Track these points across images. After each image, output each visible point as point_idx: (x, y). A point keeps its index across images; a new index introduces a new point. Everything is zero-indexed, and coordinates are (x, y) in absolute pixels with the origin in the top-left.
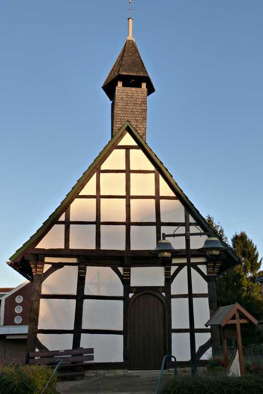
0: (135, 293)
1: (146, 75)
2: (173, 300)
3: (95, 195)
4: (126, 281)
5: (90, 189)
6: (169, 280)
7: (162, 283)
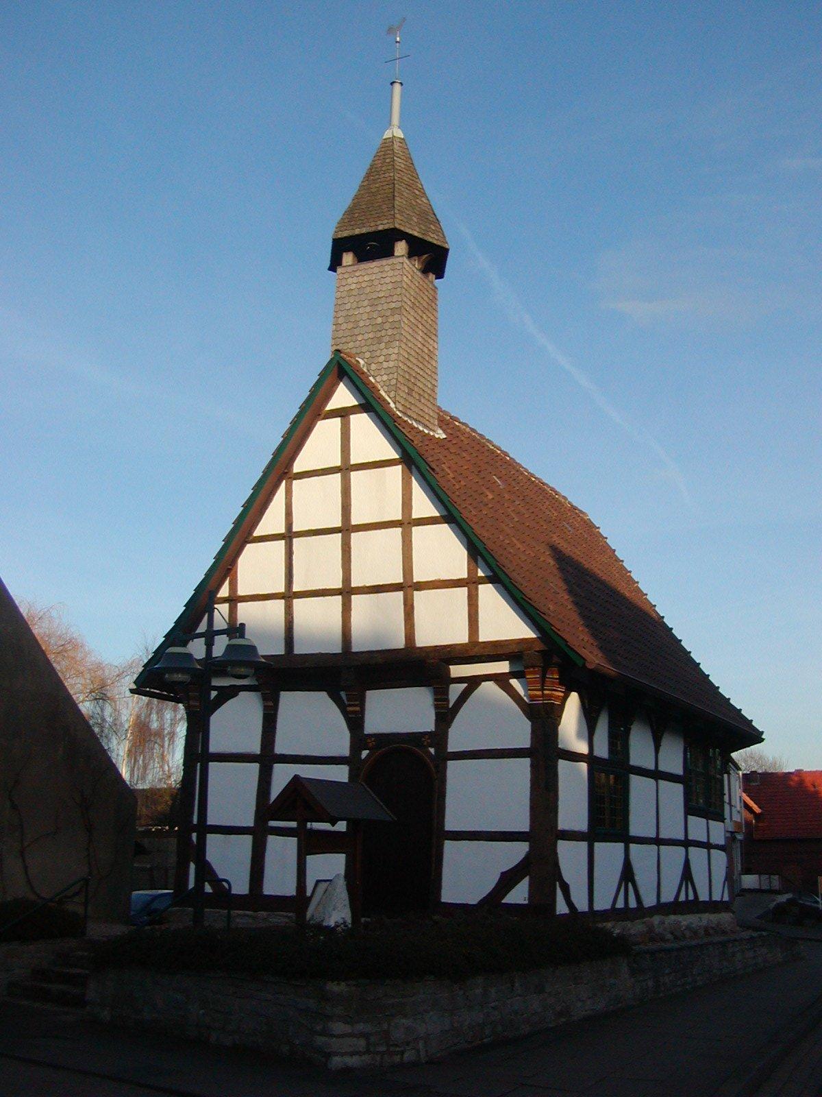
2: (451, 764)
3: (400, 518)
4: (355, 722)
5: (272, 521)
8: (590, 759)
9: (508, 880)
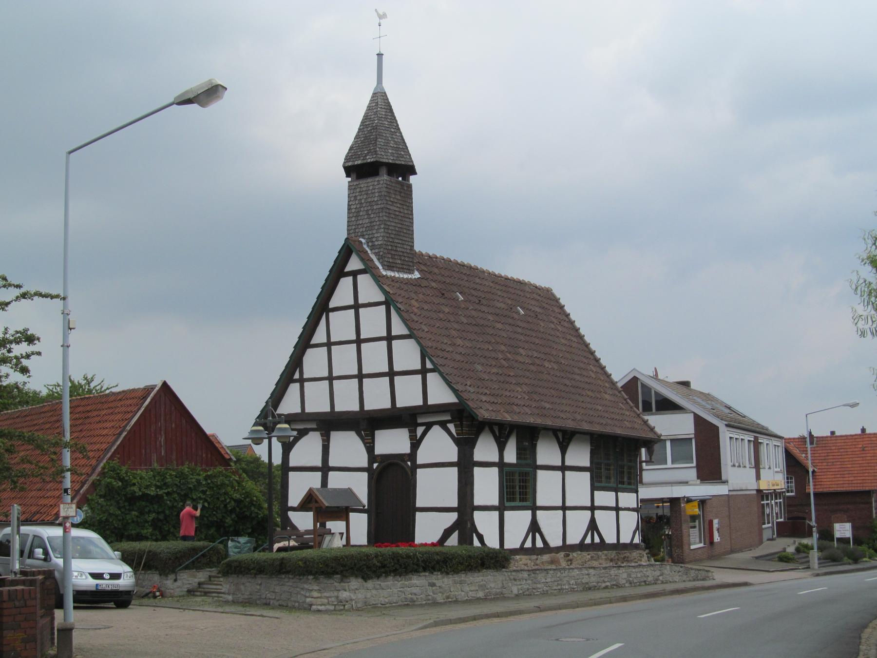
0: (380, 463)
1: (410, 164)
2: (419, 471)
4: (370, 449)
5: (320, 336)
6: (416, 444)
7: (407, 450)
8: (501, 465)
9: (447, 533)
